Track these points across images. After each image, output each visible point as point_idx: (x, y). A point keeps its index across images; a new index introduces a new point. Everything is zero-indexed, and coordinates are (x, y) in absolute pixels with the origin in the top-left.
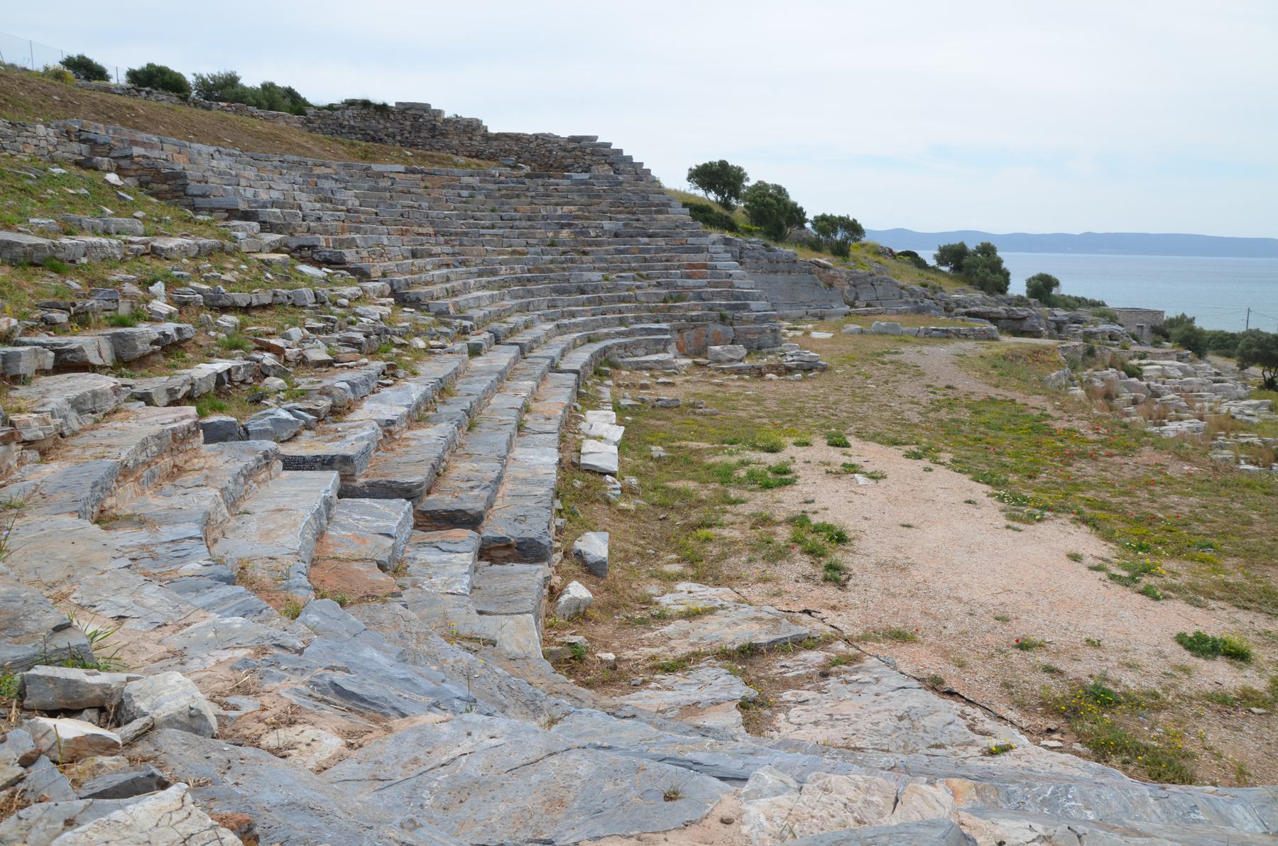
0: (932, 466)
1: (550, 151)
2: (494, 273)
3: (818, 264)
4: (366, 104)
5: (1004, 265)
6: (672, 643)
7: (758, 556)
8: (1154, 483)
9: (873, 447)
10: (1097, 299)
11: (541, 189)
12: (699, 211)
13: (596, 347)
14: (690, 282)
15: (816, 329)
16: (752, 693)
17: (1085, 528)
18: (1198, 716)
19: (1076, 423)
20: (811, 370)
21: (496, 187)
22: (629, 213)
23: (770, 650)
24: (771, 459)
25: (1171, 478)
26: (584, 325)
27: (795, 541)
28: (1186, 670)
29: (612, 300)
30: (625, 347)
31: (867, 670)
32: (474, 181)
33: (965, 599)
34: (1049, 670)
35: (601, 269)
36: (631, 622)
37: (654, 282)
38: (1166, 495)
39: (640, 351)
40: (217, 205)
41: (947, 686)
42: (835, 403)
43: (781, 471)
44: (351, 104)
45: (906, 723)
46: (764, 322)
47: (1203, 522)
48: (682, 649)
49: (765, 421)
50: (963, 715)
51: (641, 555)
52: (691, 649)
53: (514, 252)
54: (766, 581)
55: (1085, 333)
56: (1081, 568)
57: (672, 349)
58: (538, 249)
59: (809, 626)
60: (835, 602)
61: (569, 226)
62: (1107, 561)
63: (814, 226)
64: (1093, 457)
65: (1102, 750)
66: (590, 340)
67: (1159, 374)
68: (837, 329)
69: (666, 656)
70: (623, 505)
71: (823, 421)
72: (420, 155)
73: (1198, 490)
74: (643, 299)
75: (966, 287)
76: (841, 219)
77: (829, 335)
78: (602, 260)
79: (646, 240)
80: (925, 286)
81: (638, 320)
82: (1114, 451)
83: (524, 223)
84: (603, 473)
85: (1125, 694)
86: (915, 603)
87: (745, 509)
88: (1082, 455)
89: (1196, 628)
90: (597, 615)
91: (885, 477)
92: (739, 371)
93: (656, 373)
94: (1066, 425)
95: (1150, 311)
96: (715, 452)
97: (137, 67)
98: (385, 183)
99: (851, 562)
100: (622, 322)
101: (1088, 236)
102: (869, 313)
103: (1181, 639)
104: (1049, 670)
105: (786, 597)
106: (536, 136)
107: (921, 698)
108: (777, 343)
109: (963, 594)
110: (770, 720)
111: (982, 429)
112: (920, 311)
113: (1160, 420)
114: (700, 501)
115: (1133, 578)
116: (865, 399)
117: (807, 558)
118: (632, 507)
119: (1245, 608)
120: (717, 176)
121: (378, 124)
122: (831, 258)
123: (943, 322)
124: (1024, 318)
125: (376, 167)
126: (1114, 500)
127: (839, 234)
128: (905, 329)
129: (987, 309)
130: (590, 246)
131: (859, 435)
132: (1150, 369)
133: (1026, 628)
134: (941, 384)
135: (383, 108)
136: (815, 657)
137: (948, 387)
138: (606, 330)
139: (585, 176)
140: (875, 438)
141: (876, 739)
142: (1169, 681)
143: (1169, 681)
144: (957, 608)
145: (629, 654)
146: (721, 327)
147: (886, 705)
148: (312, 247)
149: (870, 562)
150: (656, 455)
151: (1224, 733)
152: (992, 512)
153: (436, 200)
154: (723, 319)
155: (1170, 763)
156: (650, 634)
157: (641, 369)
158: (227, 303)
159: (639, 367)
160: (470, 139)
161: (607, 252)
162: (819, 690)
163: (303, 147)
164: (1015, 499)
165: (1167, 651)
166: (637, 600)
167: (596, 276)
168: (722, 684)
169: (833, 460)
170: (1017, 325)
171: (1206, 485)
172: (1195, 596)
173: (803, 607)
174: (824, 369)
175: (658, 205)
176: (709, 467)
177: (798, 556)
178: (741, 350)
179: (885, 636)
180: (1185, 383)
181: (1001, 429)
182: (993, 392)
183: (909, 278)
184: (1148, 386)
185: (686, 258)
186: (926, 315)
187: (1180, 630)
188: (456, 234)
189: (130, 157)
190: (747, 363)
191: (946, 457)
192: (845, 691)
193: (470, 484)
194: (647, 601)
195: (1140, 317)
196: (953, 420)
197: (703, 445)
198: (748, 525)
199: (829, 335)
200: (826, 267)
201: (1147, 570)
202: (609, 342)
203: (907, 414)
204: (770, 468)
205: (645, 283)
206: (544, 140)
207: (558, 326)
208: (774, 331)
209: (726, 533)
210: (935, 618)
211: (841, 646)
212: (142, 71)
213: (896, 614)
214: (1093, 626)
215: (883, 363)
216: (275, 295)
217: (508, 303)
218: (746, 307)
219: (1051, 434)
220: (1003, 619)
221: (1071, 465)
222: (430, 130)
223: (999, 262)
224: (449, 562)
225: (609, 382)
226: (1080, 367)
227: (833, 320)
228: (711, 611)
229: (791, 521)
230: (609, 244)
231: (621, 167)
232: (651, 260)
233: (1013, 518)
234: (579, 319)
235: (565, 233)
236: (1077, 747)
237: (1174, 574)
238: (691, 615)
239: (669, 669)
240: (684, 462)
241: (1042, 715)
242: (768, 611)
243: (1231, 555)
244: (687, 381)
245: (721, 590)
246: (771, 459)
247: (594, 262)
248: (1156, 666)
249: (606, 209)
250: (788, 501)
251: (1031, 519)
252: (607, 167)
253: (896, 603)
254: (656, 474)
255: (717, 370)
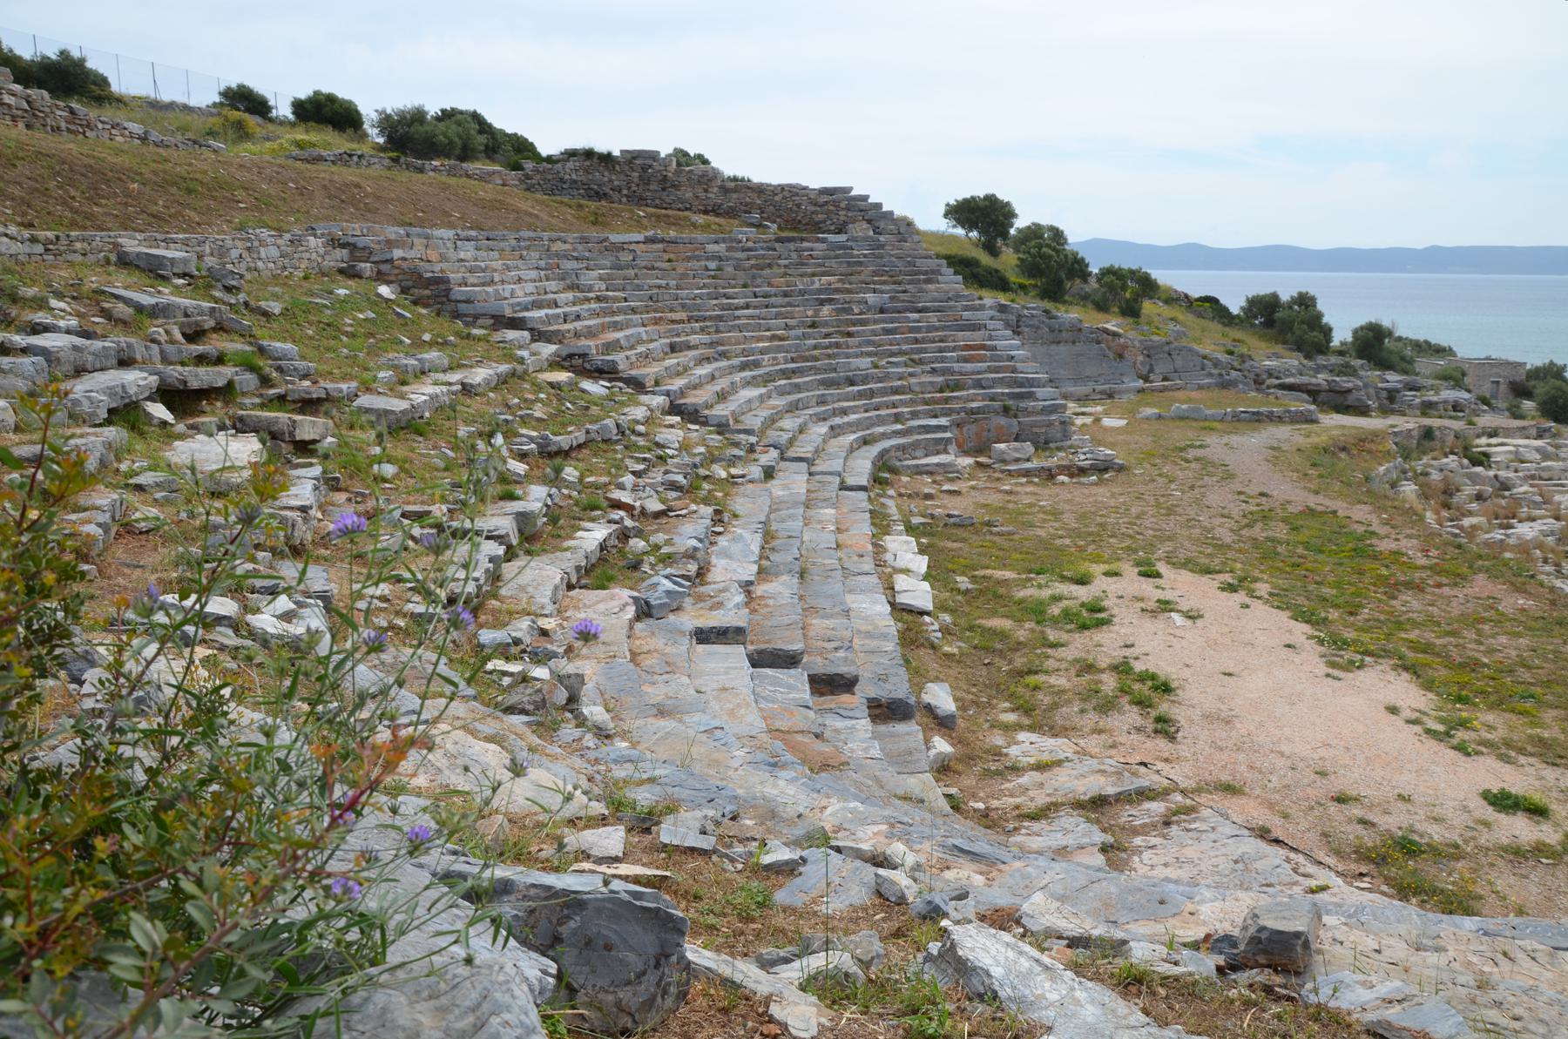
0: (1248, 600)
1: (799, 206)
2: (756, 364)
3: (1106, 331)
4: (589, 154)
5: (1325, 320)
6: (1031, 793)
7: (1088, 706)
8: (1483, 620)
9: (1185, 577)
10: (1445, 344)
11: (794, 255)
12: (963, 265)
13: (875, 450)
14: (969, 366)
15: (1107, 413)
16: (1109, 839)
17: (1406, 676)
18: (1492, 865)
19: (1404, 542)
20: (1106, 470)
21: (745, 254)
22: (895, 283)
23: (1117, 801)
24: (1082, 593)
25: (1503, 614)
26: (857, 425)
27: (1122, 690)
28: (1487, 824)
29: (884, 392)
30: (902, 448)
31: (1204, 820)
32: (720, 248)
33: (1287, 753)
34: (1363, 822)
35: (869, 354)
36: (987, 774)
37: (928, 368)
38: (1493, 636)
39: (919, 453)
40: (481, 311)
41: (1274, 835)
42: (1138, 517)
43: (1095, 608)
44: (571, 154)
45: (1240, 866)
46: (1051, 412)
47: (1529, 668)
48: (1041, 799)
49: (1067, 541)
50: (1288, 860)
51: (976, 703)
52: (1049, 800)
53: (773, 338)
54: (1101, 732)
55: (1423, 403)
56: (1398, 721)
57: (952, 448)
58: (799, 332)
59: (1147, 779)
60: (1166, 755)
61: (830, 301)
62: (1425, 713)
63: (1099, 280)
64: (1419, 588)
65: (1404, 892)
66: (866, 442)
67: (1512, 457)
68: (1130, 412)
69: (1030, 807)
70: (947, 649)
71: (1128, 542)
72: (652, 215)
73: (1530, 629)
74: (917, 389)
75: (1279, 348)
76: (1132, 272)
77: (1123, 422)
78: (869, 343)
79: (915, 316)
80: (1231, 353)
81: (915, 415)
82: (1444, 580)
83: (780, 300)
84: (922, 613)
85: (1428, 845)
86: (1241, 757)
87: (1068, 653)
88: (1409, 585)
89: (1501, 785)
90: (960, 767)
91: (1201, 616)
92: (1027, 473)
93: (939, 478)
94: (1393, 546)
95: (1508, 363)
96: (1024, 584)
97: (303, 96)
98: (626, 257)
99: (1178, 713)
100: (897, 418)
101: (1434, 250)
102: (1165, 389)
103: (1487, 796)
104: (1363, 822)
105: (1122, 749)
106: (782, 188)
107: (1252, 845)
108: (1066, 436)
109: (1285, 748)
110: (1127, 862)
111: (1300, 550)
112: (1225, 385)
113: (1506, 518)
114: (1019, 643)
115: (1447, 734)
116: (1171, 511)
117: (1135, 709)
118: (956, 651)
119: (1554, 764)
120: (985, 215)
121: (601, 176)
122: (1120, 320)
123: (1253, 401)
124: (1349, 391)
125: (615, 238)
126: (1439, 642)
127: (1128, 290)
128: (1209, 412)
129: (1305, 379)
130: (854, 325)
131: (1169, 560)
132: (1501, 450)
133: (1344, 782)
134: (1253, 490)
135: (607, 158)
136: (1157, 807)
137: (1262, 494)
138: (881, 429)
139: (842, 238)
140: (1187, 564)
141: (1217, 878)
142: (1470, 834)
143: (1470, 834)
144: (1280, 763)
145: (995, 803)
146: (1003, 423)
147: (1223, 851)
148: (583, 356)
149: (1196, 714)
150: (963, 587)
151: (1512, 880)
152: (1311, 658)
153: (683, 276)
154: (1006, 410)
155: (1460, 903)
156: (1008, 785)
157: (920, 473)
158: (554, 448)
159: (919, 471)
160: (706, 191)
161: (874, 333)
162: (1164, 837)
163: (531, 214)
164: (1335, 643)
165: (1472, 806)
166: (988, 751)
167: (865, 362)
168: (1077, 830)
169: (1146, 594)
170: (1339, 399)
171: (1541, 624)
172: (1505, 751)
173: (1138, 759)
174: (1121, 469)
175: (926, 273)
176: (1021, 602)
177: (1127, 707)
178: (1028, 447)
179: (1216, 789)
180: (1544, 469)
181: (1321, 552)
182: (1313, 501)
183: (1210, 342)
184: (1496, 477)
185: (964, 338)
186: (1233, 391)
187: (1487, 786)
188: (711, 318)
189: (390, 261)
190: (1034, 464)
191: (1263, 588)
192: (1187, 838)
193: (834, 644)
194: (997, 753)
195: (1495, 370)
196: (1268, 539)
197: (1009, 574)
198: (1073, 672)
199: (1123, 422)
200: (1115, 334)
201: (1463, 724)
202: (887, 444)
203: (1219, 532)
204: (1083, 605)
205: (918, 369)
206: (792, 192)
207: (832, 428)
208: (1063, 423)
209: (1053, 680)
210: (1260, 772)
211: (1178, 798)
212: (310, 100)
213: (1224, 767)
214: (1405, 781)
215: (1187, 461)
216: (588, 432)
217: (779, 402)
218: (1031, 396)
219: (1375, 558)
220: (1323, 774)
221: (1395, 598)
222: (660, 182)
223: (1319, 316)
224: (853, 727)
225: (891, 492)
226: (1414, 455)
227: (1125, 398)
228: (1059, 763)
229: (1114, 668)
230: (876, 322)
231: (882, 225)
232: (923, 341)
233: (1333, 665)
234: (853, 417)
235: (826, 310)
236: (1384, 888)
237: (1491, 728)
238: (1041, 767)
239: (1034, 817)
240: (992, 595)
241: (1356, 861)
242: (1110, 764)
243: (1551, 706)
244: (973, 488)
245: (1061, 741)
246: (1082, 593)
247: (860, 345)
248: (1460, 820)
249: (869, 279)
250: (1106, 645)
251: (1350, 666)
252: (865, 225)
253: (1225, 756)
254: (967, 609)
255: (1002, 471)
